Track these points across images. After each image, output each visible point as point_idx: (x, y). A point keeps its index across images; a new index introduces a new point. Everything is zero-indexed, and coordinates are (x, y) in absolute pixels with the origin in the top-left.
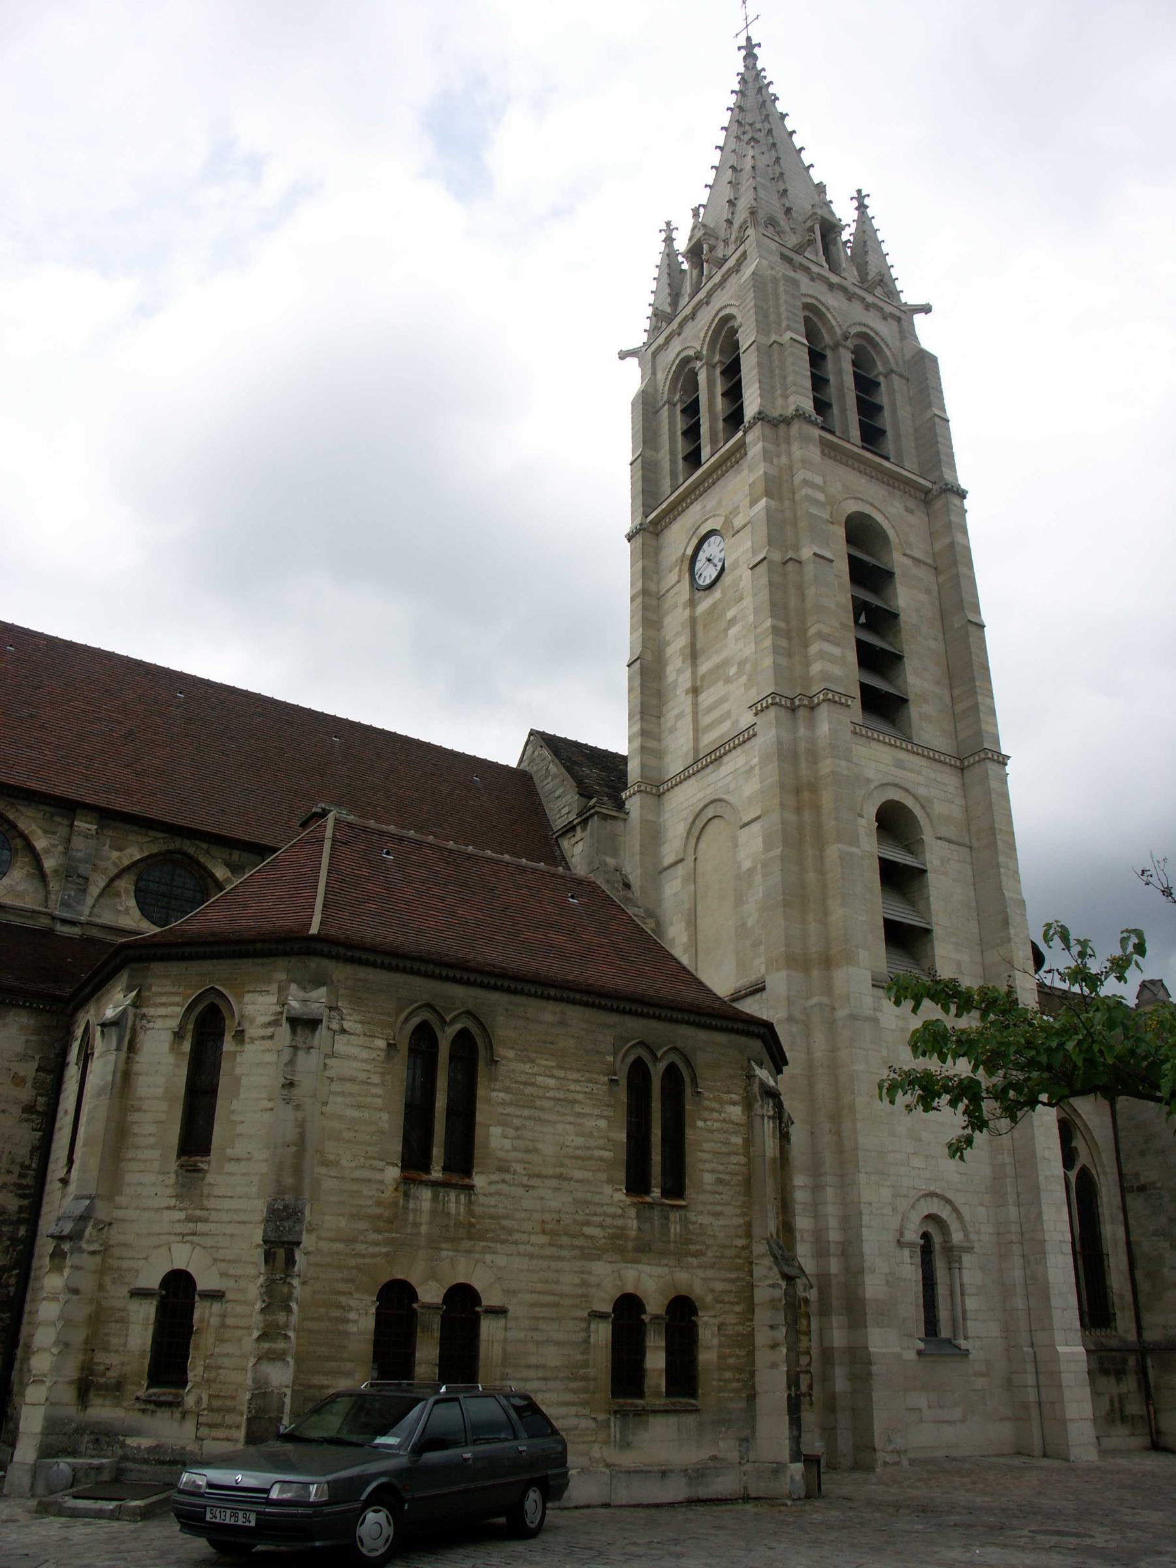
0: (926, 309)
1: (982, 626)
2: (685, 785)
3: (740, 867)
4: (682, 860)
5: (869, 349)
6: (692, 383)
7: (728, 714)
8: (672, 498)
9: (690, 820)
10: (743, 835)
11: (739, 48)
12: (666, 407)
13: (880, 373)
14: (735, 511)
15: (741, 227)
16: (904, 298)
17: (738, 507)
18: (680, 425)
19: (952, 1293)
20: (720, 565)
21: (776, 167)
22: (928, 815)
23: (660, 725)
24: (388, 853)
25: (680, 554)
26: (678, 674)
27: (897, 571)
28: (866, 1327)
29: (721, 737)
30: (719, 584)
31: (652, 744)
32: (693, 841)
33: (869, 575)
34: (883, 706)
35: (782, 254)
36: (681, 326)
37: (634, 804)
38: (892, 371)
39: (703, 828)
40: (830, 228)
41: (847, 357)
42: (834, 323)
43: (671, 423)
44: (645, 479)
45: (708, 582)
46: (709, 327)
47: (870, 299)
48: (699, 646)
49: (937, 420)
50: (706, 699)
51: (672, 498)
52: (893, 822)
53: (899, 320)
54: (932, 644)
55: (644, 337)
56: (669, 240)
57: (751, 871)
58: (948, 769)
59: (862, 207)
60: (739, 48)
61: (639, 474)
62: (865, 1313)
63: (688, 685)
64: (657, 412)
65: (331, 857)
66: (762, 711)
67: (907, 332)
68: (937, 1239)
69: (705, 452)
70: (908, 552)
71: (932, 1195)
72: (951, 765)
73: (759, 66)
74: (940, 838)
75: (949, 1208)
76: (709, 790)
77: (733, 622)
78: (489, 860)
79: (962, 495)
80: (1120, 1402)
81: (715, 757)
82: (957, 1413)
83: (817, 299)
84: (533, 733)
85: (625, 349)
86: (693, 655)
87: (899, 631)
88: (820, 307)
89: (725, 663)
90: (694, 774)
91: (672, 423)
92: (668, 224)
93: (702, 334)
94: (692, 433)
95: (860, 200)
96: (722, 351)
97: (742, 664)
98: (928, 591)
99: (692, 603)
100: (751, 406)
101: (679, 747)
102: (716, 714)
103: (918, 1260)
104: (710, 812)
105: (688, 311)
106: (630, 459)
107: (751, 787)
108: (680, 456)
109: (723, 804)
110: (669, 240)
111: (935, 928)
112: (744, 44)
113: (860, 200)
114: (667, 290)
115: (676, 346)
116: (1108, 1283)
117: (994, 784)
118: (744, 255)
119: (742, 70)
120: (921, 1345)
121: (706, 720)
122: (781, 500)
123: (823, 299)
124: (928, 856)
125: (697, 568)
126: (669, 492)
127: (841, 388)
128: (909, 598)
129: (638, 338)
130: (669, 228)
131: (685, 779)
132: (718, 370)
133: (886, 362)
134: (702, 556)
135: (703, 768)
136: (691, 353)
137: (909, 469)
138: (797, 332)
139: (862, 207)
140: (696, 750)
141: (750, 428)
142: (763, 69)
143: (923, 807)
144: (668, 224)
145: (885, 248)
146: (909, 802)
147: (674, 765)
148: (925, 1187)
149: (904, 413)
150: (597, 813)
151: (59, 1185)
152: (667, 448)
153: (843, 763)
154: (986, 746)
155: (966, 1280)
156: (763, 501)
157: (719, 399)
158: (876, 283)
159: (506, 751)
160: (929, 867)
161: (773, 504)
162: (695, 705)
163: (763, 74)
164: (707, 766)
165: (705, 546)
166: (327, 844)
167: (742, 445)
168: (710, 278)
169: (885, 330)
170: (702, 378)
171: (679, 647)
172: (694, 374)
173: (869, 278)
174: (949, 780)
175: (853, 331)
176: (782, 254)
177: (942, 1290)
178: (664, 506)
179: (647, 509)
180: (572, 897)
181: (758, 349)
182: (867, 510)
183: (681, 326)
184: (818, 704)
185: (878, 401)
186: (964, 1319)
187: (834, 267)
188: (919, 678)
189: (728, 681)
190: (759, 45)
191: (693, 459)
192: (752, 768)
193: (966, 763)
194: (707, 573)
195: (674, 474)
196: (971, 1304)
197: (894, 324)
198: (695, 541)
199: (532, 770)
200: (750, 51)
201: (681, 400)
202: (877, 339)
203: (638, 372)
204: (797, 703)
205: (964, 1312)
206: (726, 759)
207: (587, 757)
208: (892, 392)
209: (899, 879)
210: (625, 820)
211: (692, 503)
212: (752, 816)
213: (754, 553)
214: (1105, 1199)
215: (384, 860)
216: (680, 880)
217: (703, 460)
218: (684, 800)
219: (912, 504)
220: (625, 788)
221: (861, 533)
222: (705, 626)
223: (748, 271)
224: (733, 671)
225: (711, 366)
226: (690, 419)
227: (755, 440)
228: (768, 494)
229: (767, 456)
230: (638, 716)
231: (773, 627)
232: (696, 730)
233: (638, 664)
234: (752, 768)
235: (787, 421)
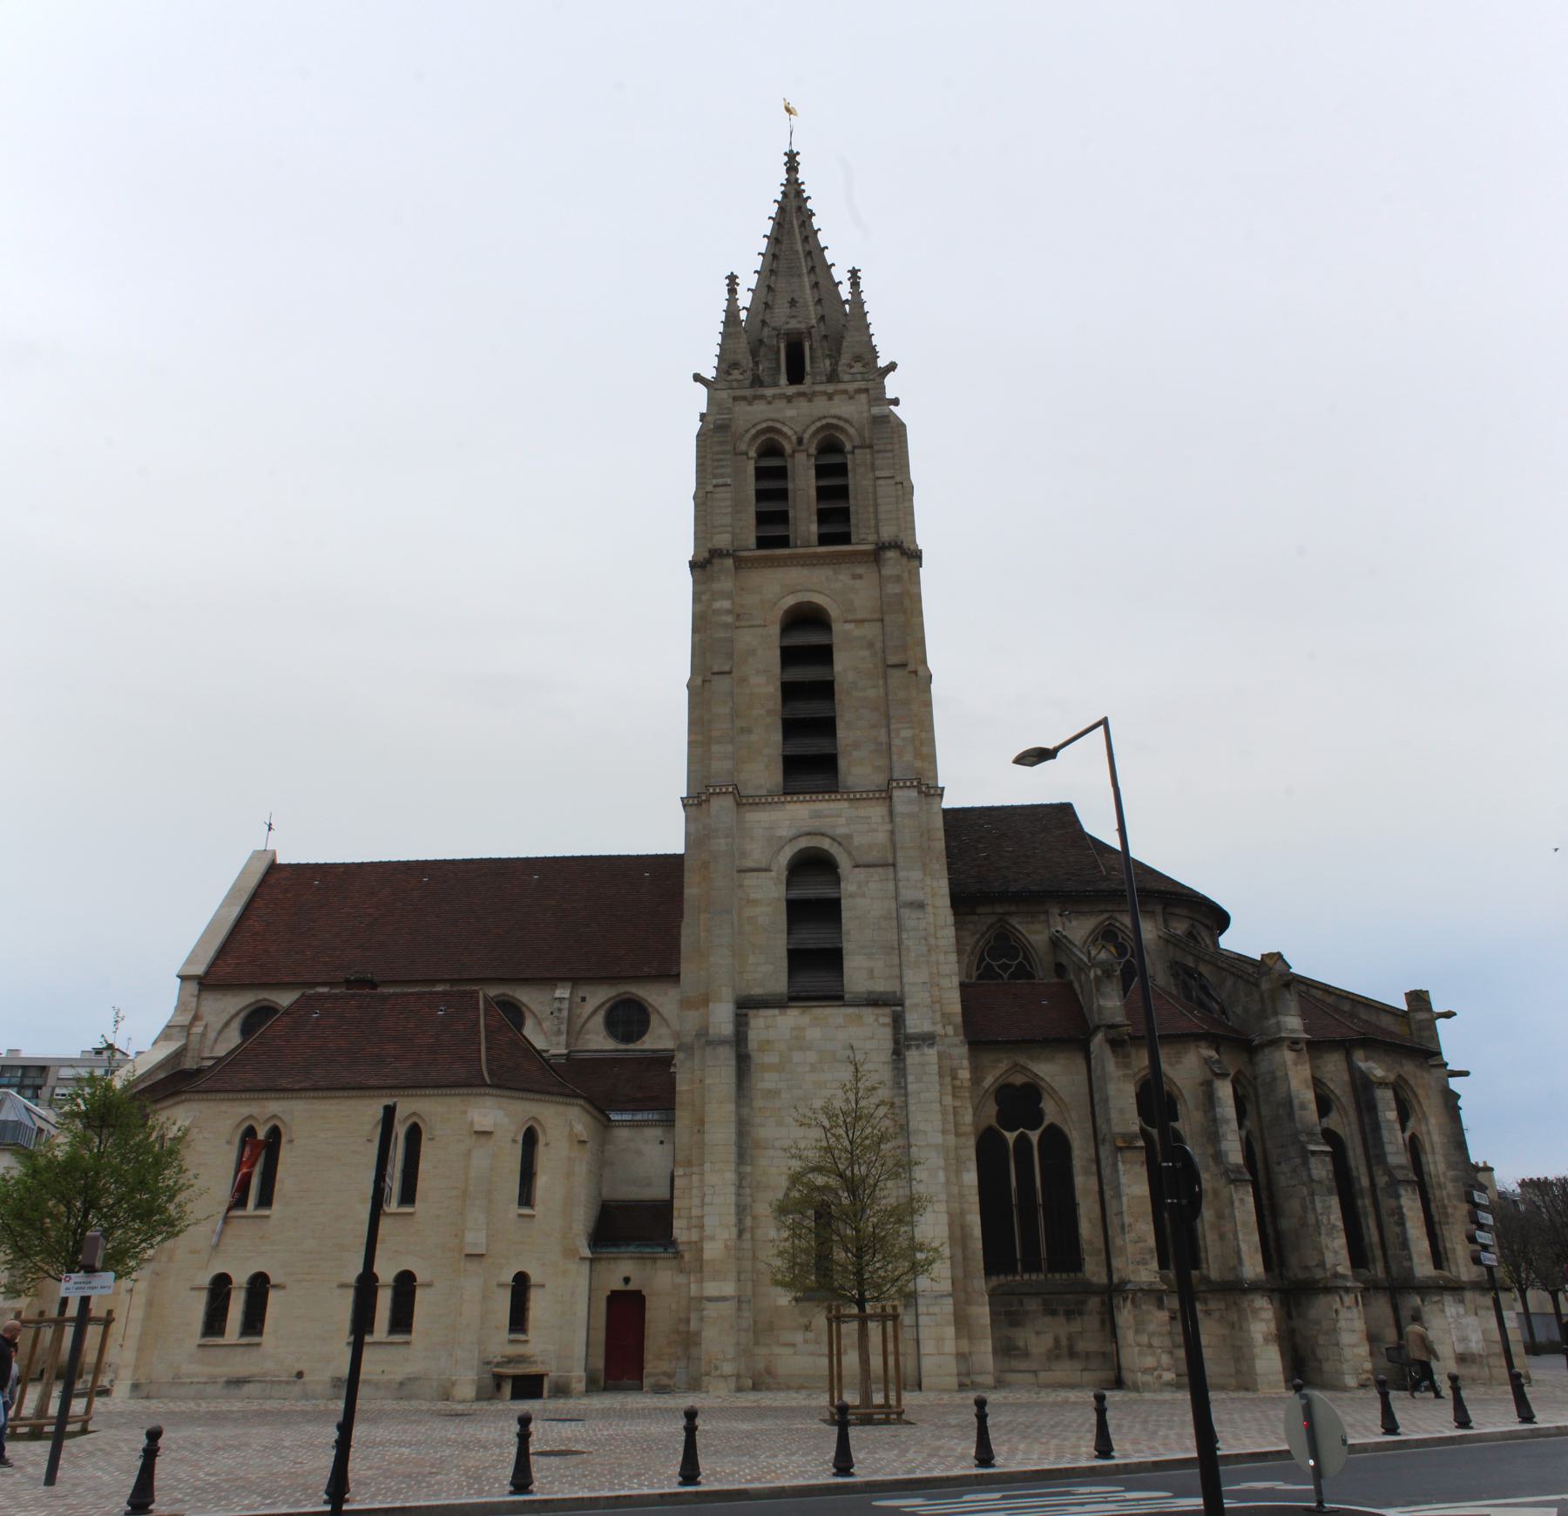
95: (854, 273)
110: (732, 291)
113: (854, 273)
130: (732, 279)
146: (826, 844)
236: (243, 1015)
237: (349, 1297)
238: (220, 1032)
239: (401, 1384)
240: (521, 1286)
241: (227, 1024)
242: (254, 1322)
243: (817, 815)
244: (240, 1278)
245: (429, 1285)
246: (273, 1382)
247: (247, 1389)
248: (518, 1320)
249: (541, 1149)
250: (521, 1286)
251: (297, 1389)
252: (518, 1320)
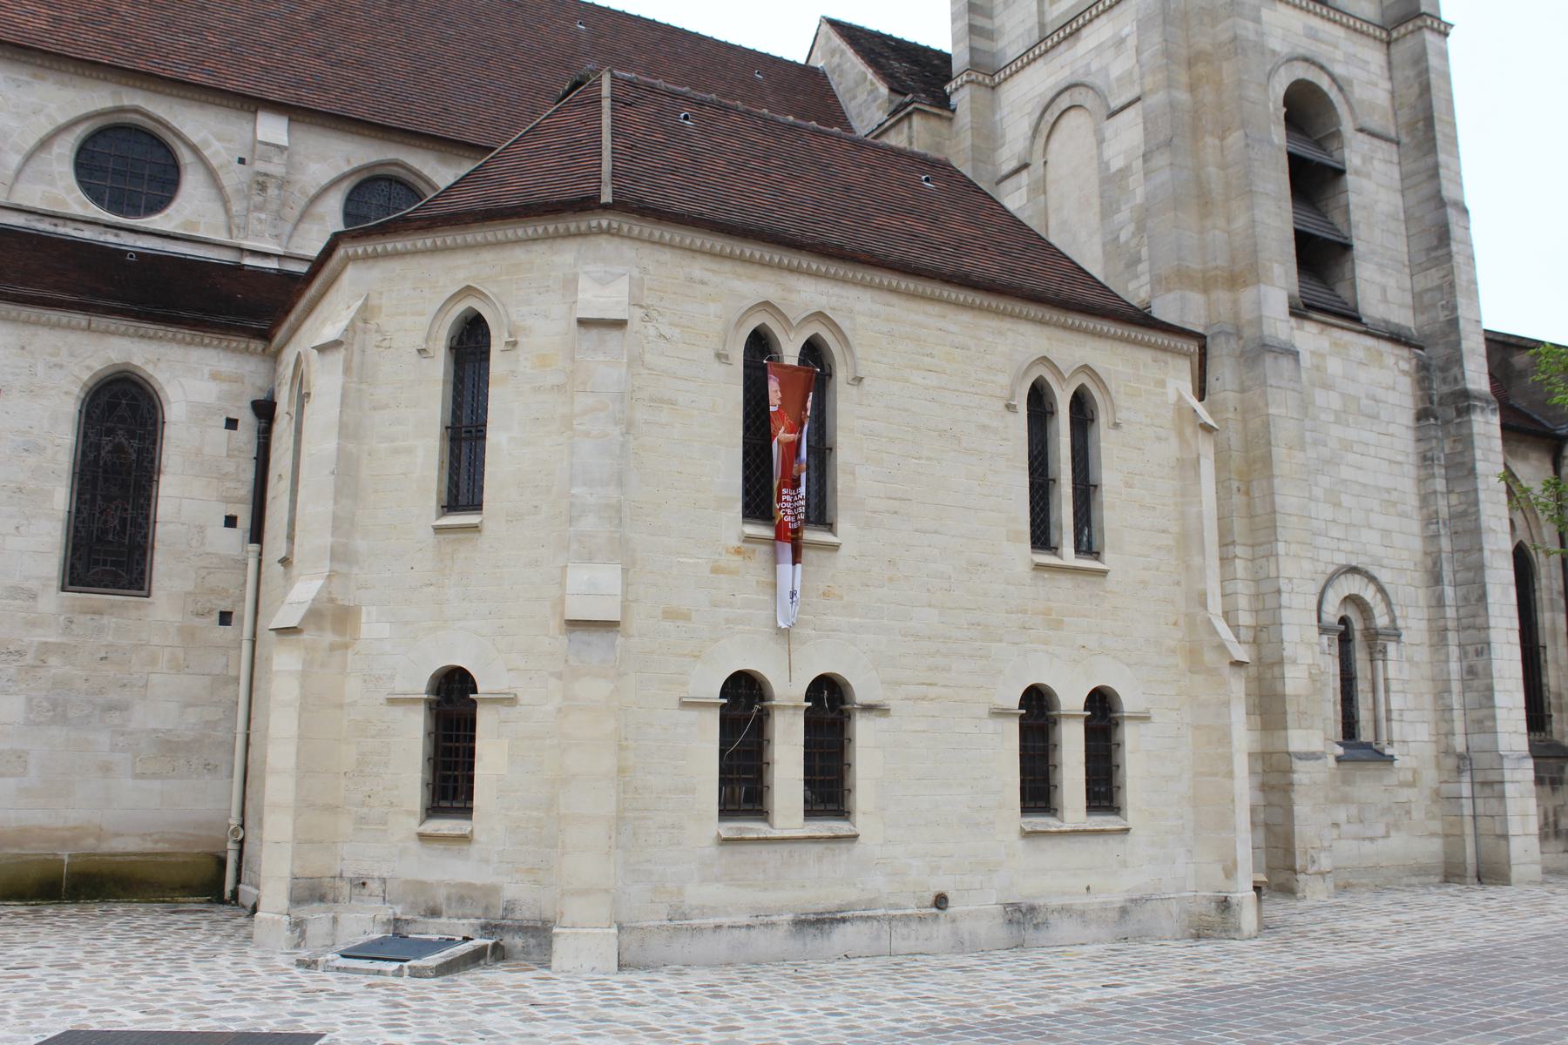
2: (1029, 70)
3: (1108, 168)
4: (1025, 166)
9: (1038, 114)
19: (1374, 690)
22: (1348, 101)
24: (686, 118)
28: (1286, 728)
31: (980, 21)
32: (1041, 141)
37: (962, 98)
39: (1055, 123)
52: (1305, 110)
57: (1124, 172)
58: (1370, 42)
62: (1285, 713)
65: (613, 120)
68: (1357, 625)
71: (1353, 570)
74: (1361, 130)
75: (1372, 588)
76: (1066, 72)
78: (816, 133)
80: (1555, 814)
82: (1380, 829)
90: (1040, 56)
103: (1335, 650)
104: (1064, 102)
107: (1121, 65)
111: (1355, 243)
116: (1544, 680)
117: (1433, 61)
120: (1340, 751)
124: (1347, 153)
131: (1029, 63)
135: (1053, 47)
140: (1042, 25)
143: (1341, 89)
146: (1324, 83)
147: (1011, 43)
148: (1342, 559)
150: (917, 109)
151: (280, 568)
154: (1423, 9)
155: (1392, 673)
164: (1059, 43)
166: (606, 104)
174: (1374, 56)
177: (1362, 686)
180: (927, 180)
186: (1389, 720)
193: (1394, 35)
196: (1396, 702)
205: (1389, 711)
206: (1085, 32)
207: (893, 49)
209: (1313, 180)
210: (950, 120)
212: (1124, 100)
214: (1544, 582)
215: (684, 126)
216: (1024, 190)
220: (949, 79)
234: (1122, 41)
236: (81, 131)
237: (1011, 732)
238: (29, 157)
239: (1124, 911)
240: (453, 704)
241: (45, 143)
242: (828, 789)
243: (1312, 35)
244: (1071, 699)
245: (1144, 718)
246: (892, 919)
247: (842, 936)
248: (450, 781)
249: (498, 363)
250: (453, 704)
251: (941, 931)
252: (450, 781)
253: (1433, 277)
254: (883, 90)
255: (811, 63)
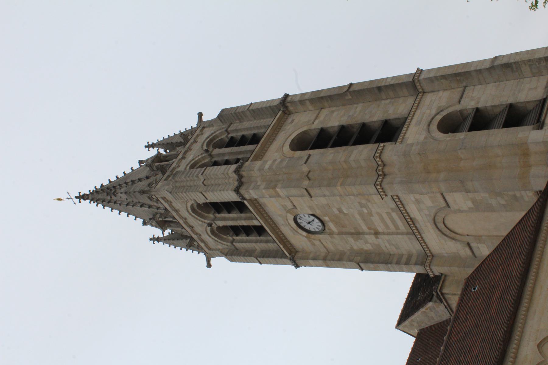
0: (200, 115)
1: (351, 85)
2: (427, 240)
4: (468, 244)
5: (215, 141)
6: (224, 230)
7: (388, 214)
8: (273, 236)
10: (453, 206)
11: (80, 202)
12: (234, 244)
13: (227, 136)
14: (284, 207)
15: (151, 200)
16: (195, 126)
17: (282, 206)
18: (243, 237)
20: (312, 218)
21: (129, 184)
22: (447, 108)
23: (394, 255)
25: (305, 239)
26: (368, 243)
27: (321, 126)
29: (400, 218)
30: (321, 218)
32: (458, 237)
33: (323, 140)
34: (389, 132)
35: (165, 180)
36: (196, 234)
37: (436, 270)
38: (226, 131)
40: (158, 158)
41: (217, 151)
42: (200, 157)
43: (243, 242)
44: (268, 257)
45: (320, 224)
46: (196, 218)
47: (192, 141)
48: (353, 231)
49: (251, 108)
50: (381, 228)
51: (273, 236)
52: (450, 125)
53: (204, 128)
54: (359, 109)
55: (202, 254)
56: (158, 239)
57: (474, 201)
58: (423, 99)
59: (153, 146)
60: (80, 202)
61: (266, 259)
63: (373, 237)
64: (237, 249)
66: (384, 192)
67: (211, 123)
69: (255, 223)
70: (312, 122)
72: (421, 98)
73: (88, 193)
77: (340, 210)
79: (287, 96)
81: (410, 222)
83: (188, 164)
84: (396, 328)
85: (205, 263)
86: (357, 234)
87: (351, 125)
88: (192, 163)
89: (361, 214)
91: (242, 241)
92: (151, 239)
93: (200, 223)
94: (247, 230)
95: (148, 146)
96: (209, 213)
97: (362, 205)
98: (333, 112)
99: (331, 234)
100: (232, 197)
101: (407, 245)
102: (389, 222)
104: (441, 226)
105: (189, 230)
106: (258, 264)
108: (258, 238)
109: (436, 218)
110: (158, 239)
112: (78, 200)
113: (148, 146)
114: (180, 241)
115: (205, 237)
118: (164, 198)
119: (88, 201)
121: (392, 228)
122: (278, 181)
123: (188, 162)
125: (313, 230)
126: (275, 244)
127: (231, 154)
128: (334, 119)
129: (202, 257)
130: (155, 239)
131: (424, 240)
132: (218, 215)
133: (221, 134)
134: (308, 227)
136: (209, 228)
137: (271, 121)
138: (199, 172)
139: (153, 146)
140: (408, 234)
141: (242, 196)
142: (90, 191)
143: (442, 111)
144: (151, 239)
145: (172, 135)
146: (439, 117)
149: (246, 124)
152: (254, 244)
153: (414, 148)
154: (411, 80)
156: (278, 190)
157: (231, 215)
158: (184, 139)
159: (407, 343)
160: (475, 106)
161: (279, 185)
162: (384, 234)
163: (91, 191)
165: (302, 225)
167: (251, 201)
168: (174, 218)
169: (207, 133)
170: (221, 224)
171: (353, 241)
172: (219, 228)
173: (183, 141)
174: (428, 99)
175: (205, 147)
176: (165, 180)
178: (281, 246)
179: (283, 256)
180: (474, 289)
181: (205, 192)
182: (289, 140)
183: (196, 234)
184: (382, 161)
185: (239, 137)
187: (176, 156)
188: (374, 114)
189: (370, 214)
190: (80, 193)
191: (260, 230)
192: (417, 200)
194: (316, 226)
195: (267, 242)
197: (205, 130)
198: (300, 231)
199: (416, 332)
200: (82, 197)
201: (232, 236)
202: (211, 137)
203: (218, 258)
204: (381, 173)
206: (412, 216)
208: (237, 131)
209: (480, 121)
210: (446, 276)
211: (281, 231)
213: (303, 196)
217: (259, 224)
218: (436, 242)
219: (290, 120)
220: (427, 275)
221: (301, 143)
222: (343, 227)
223: (169, 197)
224: (365, 211)
225: (215, 219)
226: (238, 230)
227: (250, 193)
228: (274, 187)
229: (257, 188)
230: (389, 265)
231: (341, 185)
232: (398, 234)
233: (362, 265)
234: (417, 200)
235: (240, 177)
253: (526, 69)
254: (430, 304)
255: (416, 335)
